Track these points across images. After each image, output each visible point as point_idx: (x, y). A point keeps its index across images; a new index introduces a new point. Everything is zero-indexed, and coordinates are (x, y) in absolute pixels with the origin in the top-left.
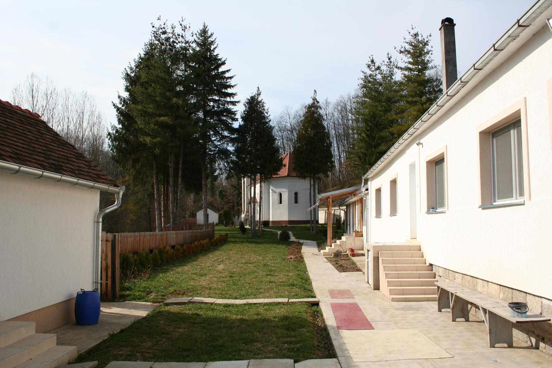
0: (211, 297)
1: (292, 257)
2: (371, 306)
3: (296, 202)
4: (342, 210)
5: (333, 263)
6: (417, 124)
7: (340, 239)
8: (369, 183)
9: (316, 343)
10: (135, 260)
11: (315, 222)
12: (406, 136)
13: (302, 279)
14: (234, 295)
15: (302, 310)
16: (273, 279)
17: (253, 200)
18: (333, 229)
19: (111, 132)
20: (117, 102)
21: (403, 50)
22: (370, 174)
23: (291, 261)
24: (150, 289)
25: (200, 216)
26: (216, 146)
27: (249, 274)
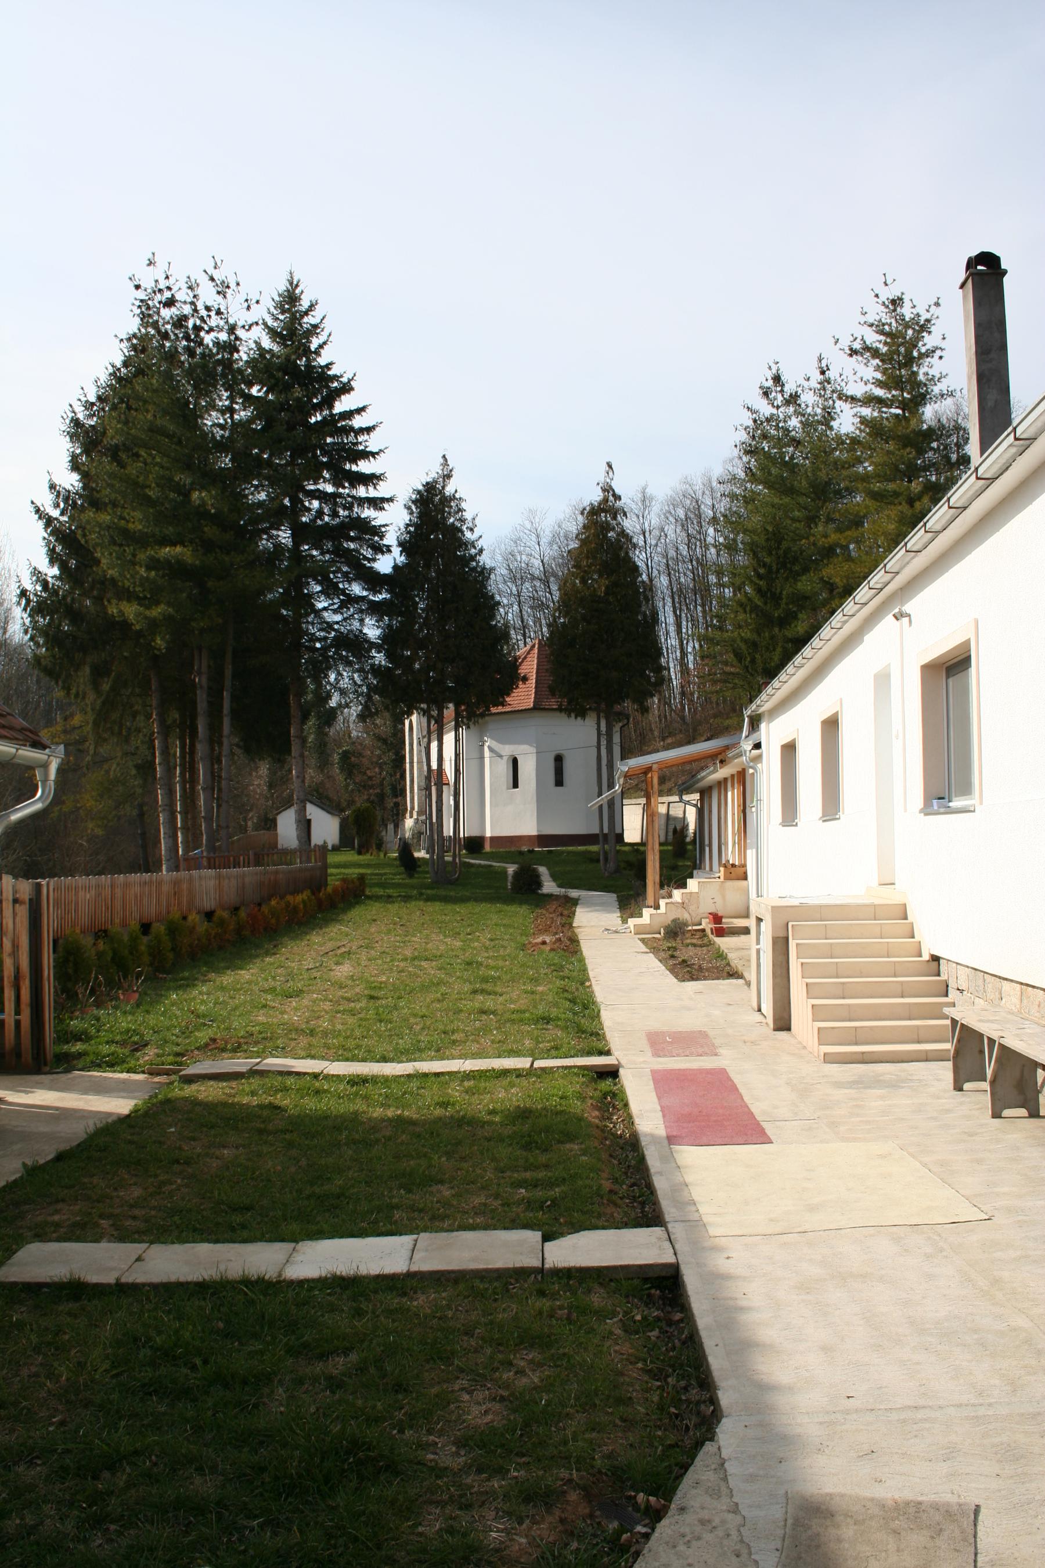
0: (313, 1057)
1: (548, 939)
2: (767, 1075)
3: (559, 782)
4: (688, 803)
5: (662, 954)
6: (896, 558)
7: (684, 885)
8: (763, 726)
9: (607, 1185)
10: (100, 955)
11: (612, 839)
12: (862, 593)
13: (573, 1001)
14: (379, 1050)
15: (570, 1090)
16: (490, 1003)
17: (435, 779)
18: (661, 860)
19: (29, 587)
20: (46, 501)
21: (857, 346)
22: (765, 701)
23: (542, 952)
24: (142, 1036)
25: (287, 826)
26: (330, 626)
27: (424, 988)
